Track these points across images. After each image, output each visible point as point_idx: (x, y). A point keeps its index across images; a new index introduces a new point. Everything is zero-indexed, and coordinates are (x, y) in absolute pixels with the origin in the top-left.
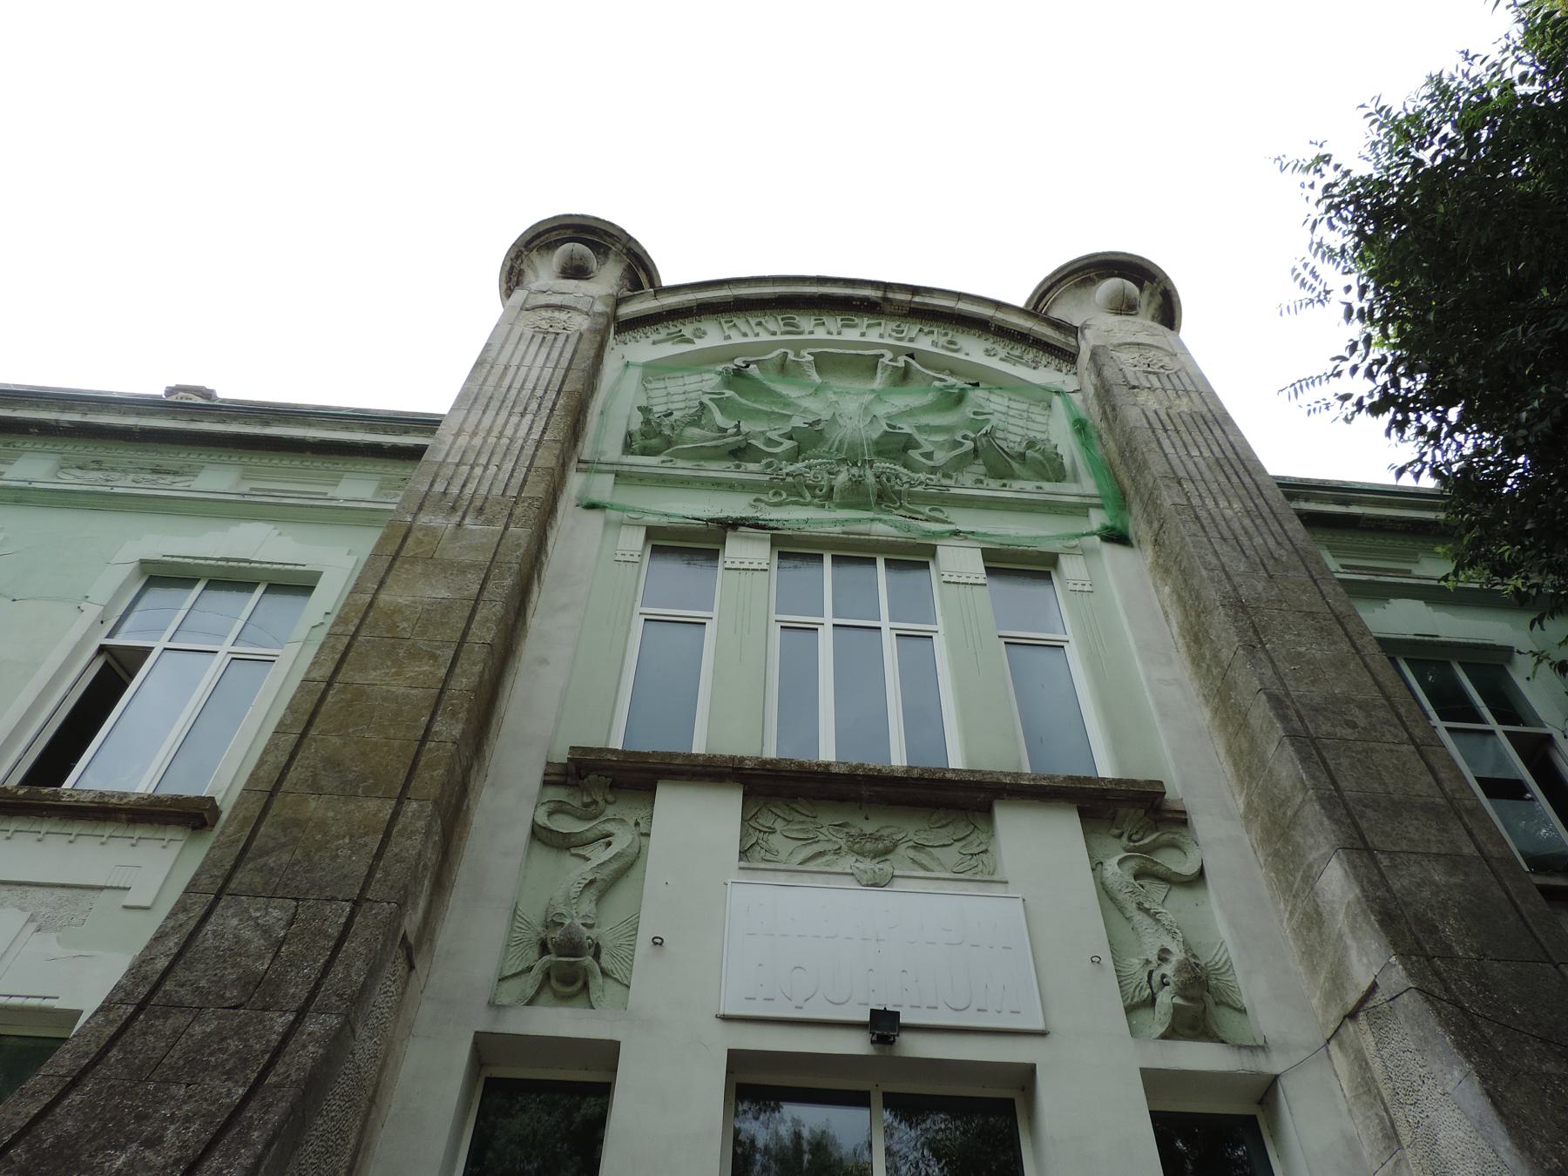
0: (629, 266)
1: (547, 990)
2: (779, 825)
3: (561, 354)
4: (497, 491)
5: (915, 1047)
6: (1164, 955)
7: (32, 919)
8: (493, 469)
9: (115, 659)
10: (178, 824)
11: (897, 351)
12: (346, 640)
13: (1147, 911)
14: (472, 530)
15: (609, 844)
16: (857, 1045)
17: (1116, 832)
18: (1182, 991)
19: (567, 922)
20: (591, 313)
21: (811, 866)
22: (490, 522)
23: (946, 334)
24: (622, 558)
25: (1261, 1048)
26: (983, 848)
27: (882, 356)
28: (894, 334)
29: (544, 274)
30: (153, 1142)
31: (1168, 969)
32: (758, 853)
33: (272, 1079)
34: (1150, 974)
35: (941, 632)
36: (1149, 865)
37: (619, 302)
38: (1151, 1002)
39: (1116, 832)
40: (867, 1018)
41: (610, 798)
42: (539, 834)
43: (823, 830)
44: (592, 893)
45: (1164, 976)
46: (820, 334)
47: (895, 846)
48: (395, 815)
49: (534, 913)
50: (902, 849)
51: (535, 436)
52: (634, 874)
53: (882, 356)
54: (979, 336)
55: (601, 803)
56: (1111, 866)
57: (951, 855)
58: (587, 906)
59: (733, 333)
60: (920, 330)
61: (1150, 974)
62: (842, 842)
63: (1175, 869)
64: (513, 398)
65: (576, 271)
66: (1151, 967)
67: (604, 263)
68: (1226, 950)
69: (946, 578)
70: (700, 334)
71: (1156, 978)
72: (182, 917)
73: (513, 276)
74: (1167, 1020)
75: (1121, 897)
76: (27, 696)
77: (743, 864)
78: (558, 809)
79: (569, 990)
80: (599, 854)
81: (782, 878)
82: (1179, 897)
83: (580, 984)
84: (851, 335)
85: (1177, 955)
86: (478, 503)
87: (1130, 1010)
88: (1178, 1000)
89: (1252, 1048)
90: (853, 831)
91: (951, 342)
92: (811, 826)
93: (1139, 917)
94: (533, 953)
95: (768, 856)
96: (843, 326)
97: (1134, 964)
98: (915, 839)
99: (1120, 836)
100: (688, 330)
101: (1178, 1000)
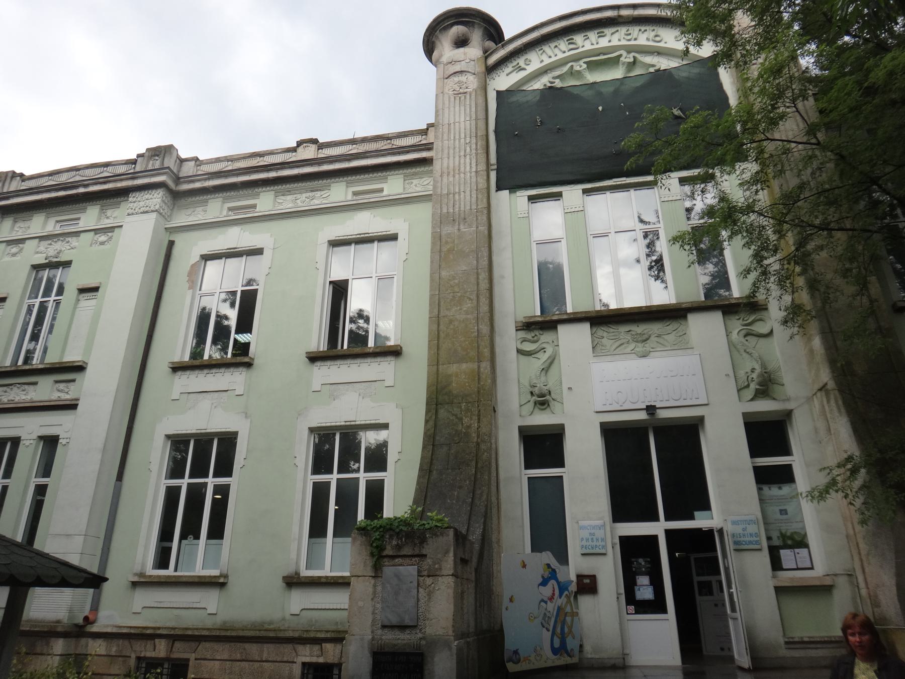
0: (485, 28)
1: (536, 407)
2: (605, 334)
3: (470, 109)
4: (468, 208)
5: (663, 414)
6: (753, 370)
7: (360, 395)
8: (462, 194)
9: (337, 285)
10: (391, 355)
11: (629, 49)
12: (437, 297)
13: (748, 353)
14: (465, 232)
15: (545, 352)
16: (643, 416)
17: (738, 317)
18: (760, 384)
19: (538, 385)
20: (476, 73)
21: (615, 352)
22: (470, 226)
23: (654, 30)
24: (521, 216)
25: (788, 400)
26: (684, 332)
27: (621, 56)
28: (626, 37)
29: (446, 50)
30: (460, 487)
31: (754, 376)
32: (598, 348)
33: (479, 465)
34: (748, 377)
35: (662, 227)
36: (750, 331)
37: (486, 58)
38: (748, 386)
39: (738, 317)
40: (645, 407)
41: (541, 332)
42: (519, 351)
43: (622, 334)
44: (544, 372)
45: (753, 378)
46: (588, 46)
47: (650, 336)
48: (479, 367)
49: (525, 382)
50: (653, 338)
51: (474, 170)
52: (556, 361)
53: (621, 56)
54: (671, 28)
55: (539, 336)
56: (734, 336)
57: (671, 338)
58: (543, 379)
59: (544, 57)
60: (640, 30)
61: (748, 377)
62: (629, 338)
63: (761, 332)
64: (458, 146)
65: (461, 42)
66: (748, 375)
67: (473, 32)
68: (779, 363)
69: (663, 199)
70: (528, 61)
71: (750, 379)
72: (430, 414)
73: (429, 47)
74: (753, 394)
75: (738, 347)
76: (317, 310)
77: (594, 355)
78: (524, 340)
79: (544, 407)
80: (544, 357)
81: (609, 358)
82: (762, 341)
83: (546, 405)
84: (604, 43)
85: (758, 370)
86: (462, 216)
87: (739, 391)
88: (758, 387)
89: (784, 400)
90: (633, 333)
91: (656, 36)
92: (617, 334)
93: (745, 354)
94: (529, 396)
95: (603, 348)
96: (599, 37)
97: (742, 374)
98: (658, 332)
99: (739, 319)
100: (521, 61)
101: (758, 387)
